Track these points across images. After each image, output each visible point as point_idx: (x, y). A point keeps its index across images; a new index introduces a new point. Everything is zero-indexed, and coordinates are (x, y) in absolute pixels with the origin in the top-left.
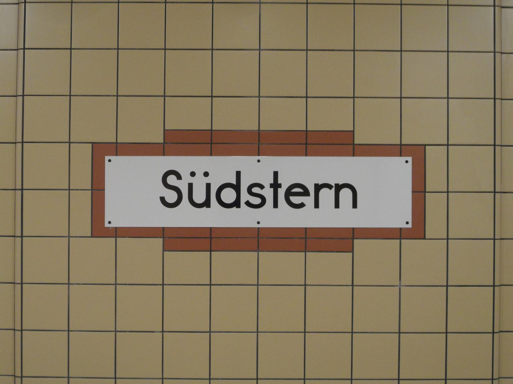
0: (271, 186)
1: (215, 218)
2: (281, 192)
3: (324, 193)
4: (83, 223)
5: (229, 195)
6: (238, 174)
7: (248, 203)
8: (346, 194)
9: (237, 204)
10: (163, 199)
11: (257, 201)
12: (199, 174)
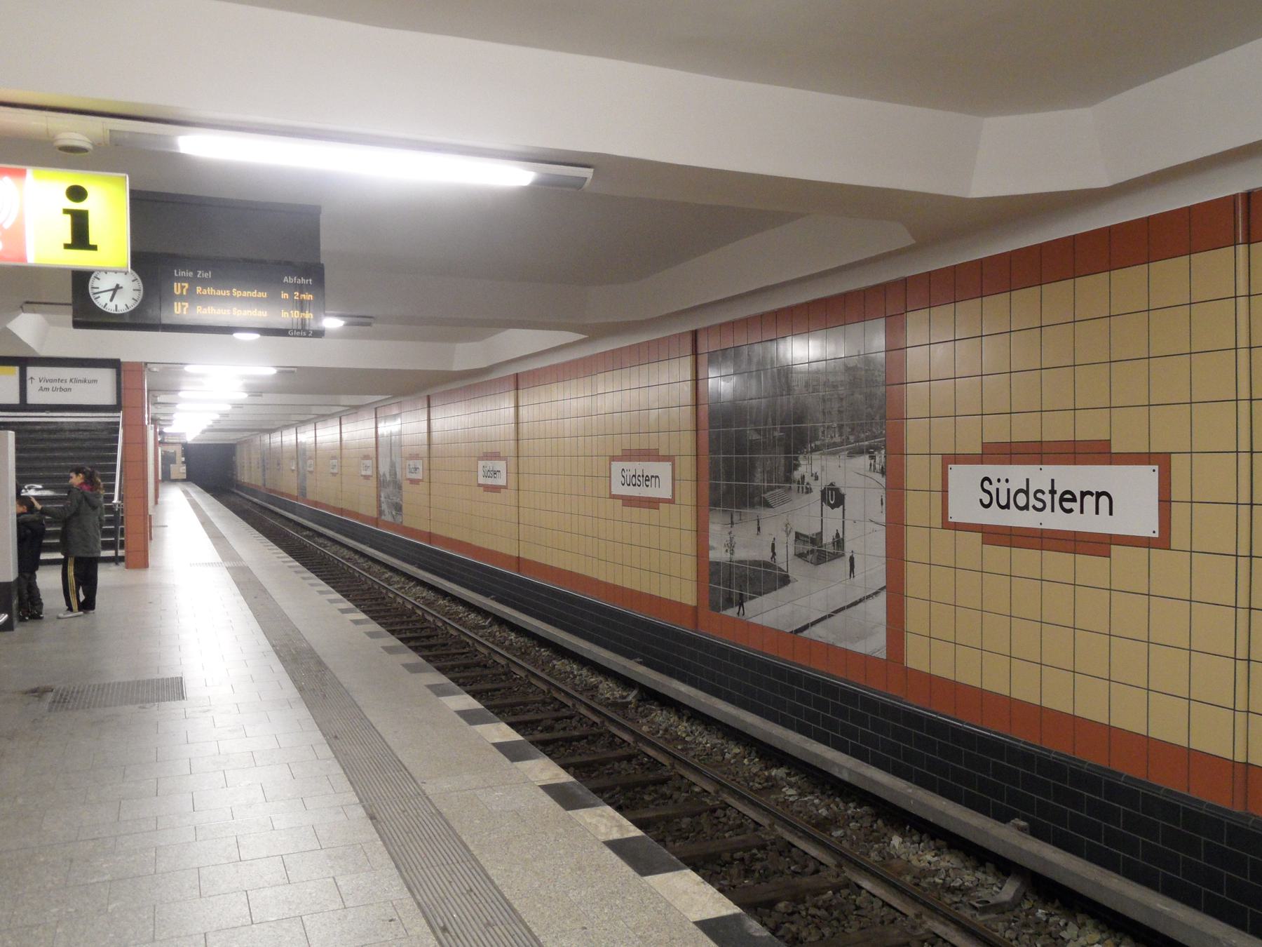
0: (302, 310)
2: (1057, 497)
4: (1179, 465)
5: (1021, 500)
7: (1034, 507)
9: (1026, 507)
11: (1040, 505)
12: (1003, 481)
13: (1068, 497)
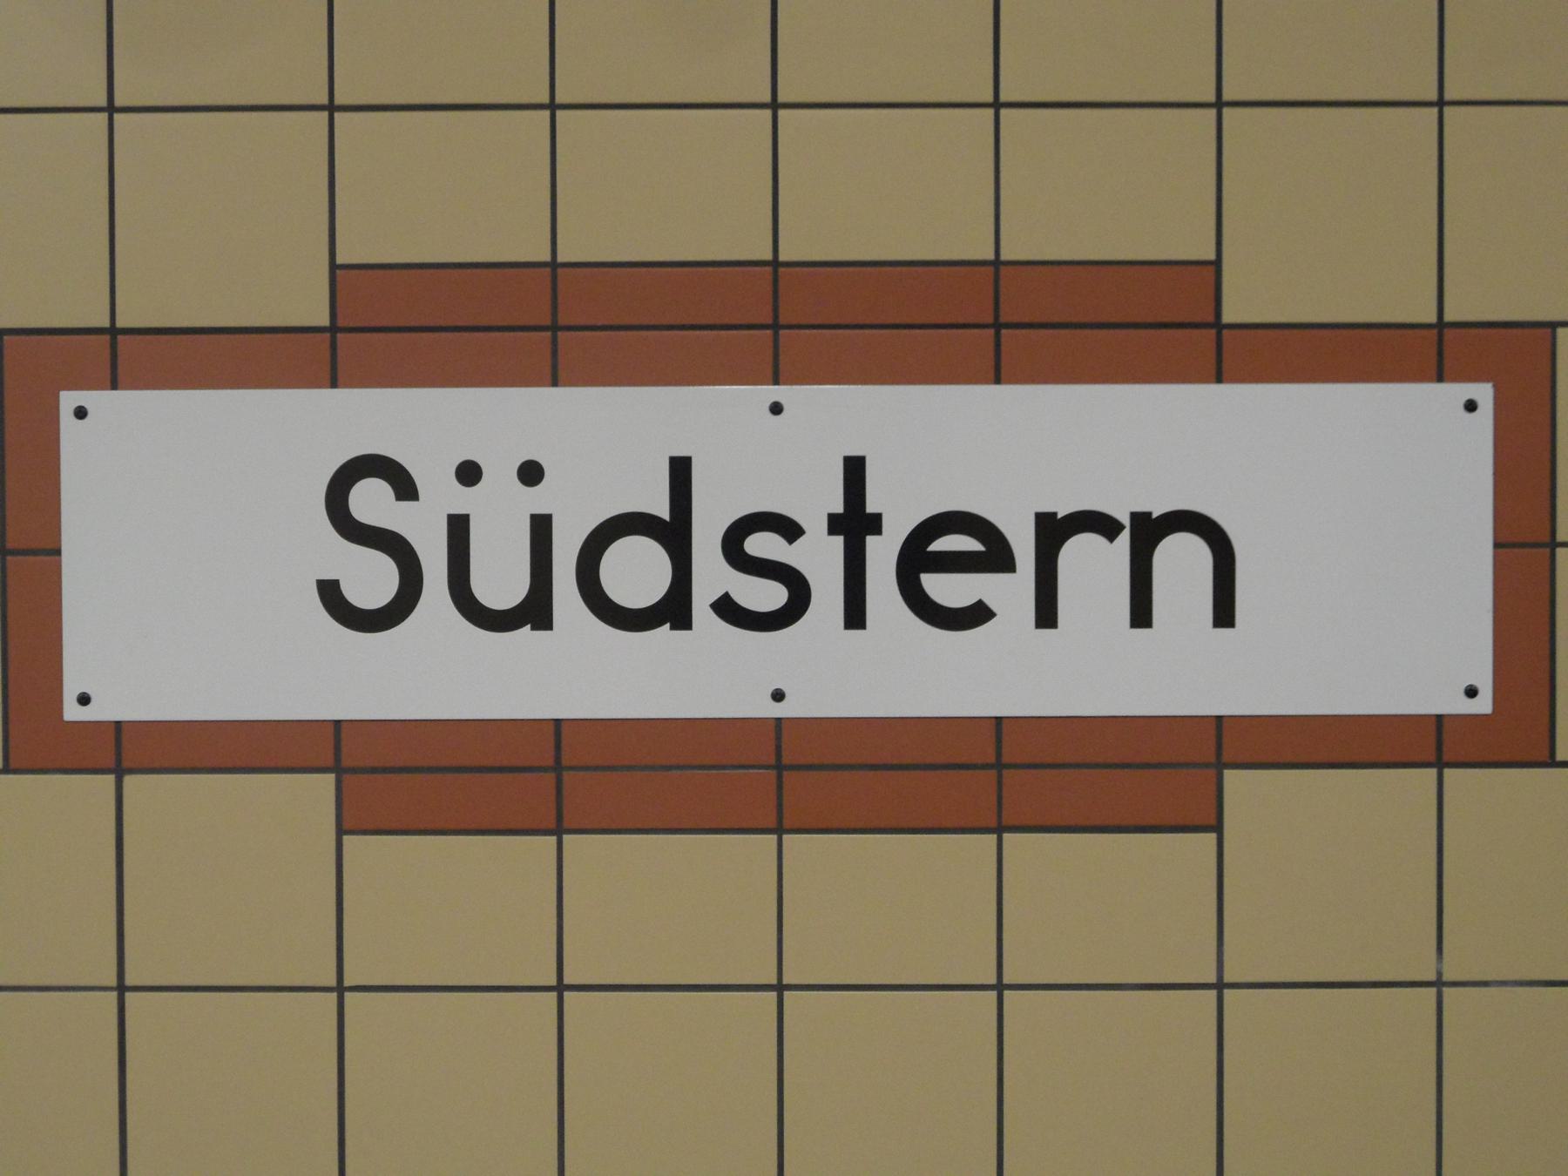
0: (835, 524)
1: (578, 674)
2: (882, 554)
3: (1079, 551)
5: (637, 572)
6: (680, 470)
7: (726, 608)
8: (1182, 564)
9: (674, 610)
10: (330, 594)
11: (767, 596)
13: (953, 544)
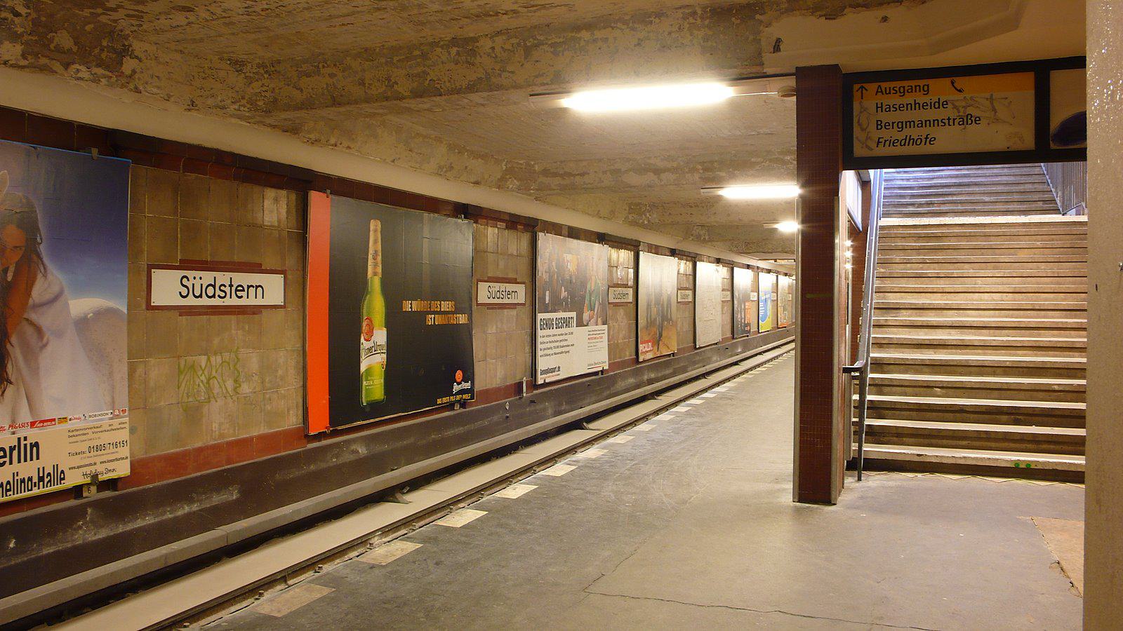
2: (234, 289)
5: (210, 291)
7: (219, 296)
9: (214, 296)
11: (223, 294)
12: (198, 278)
13: (240, 288)
